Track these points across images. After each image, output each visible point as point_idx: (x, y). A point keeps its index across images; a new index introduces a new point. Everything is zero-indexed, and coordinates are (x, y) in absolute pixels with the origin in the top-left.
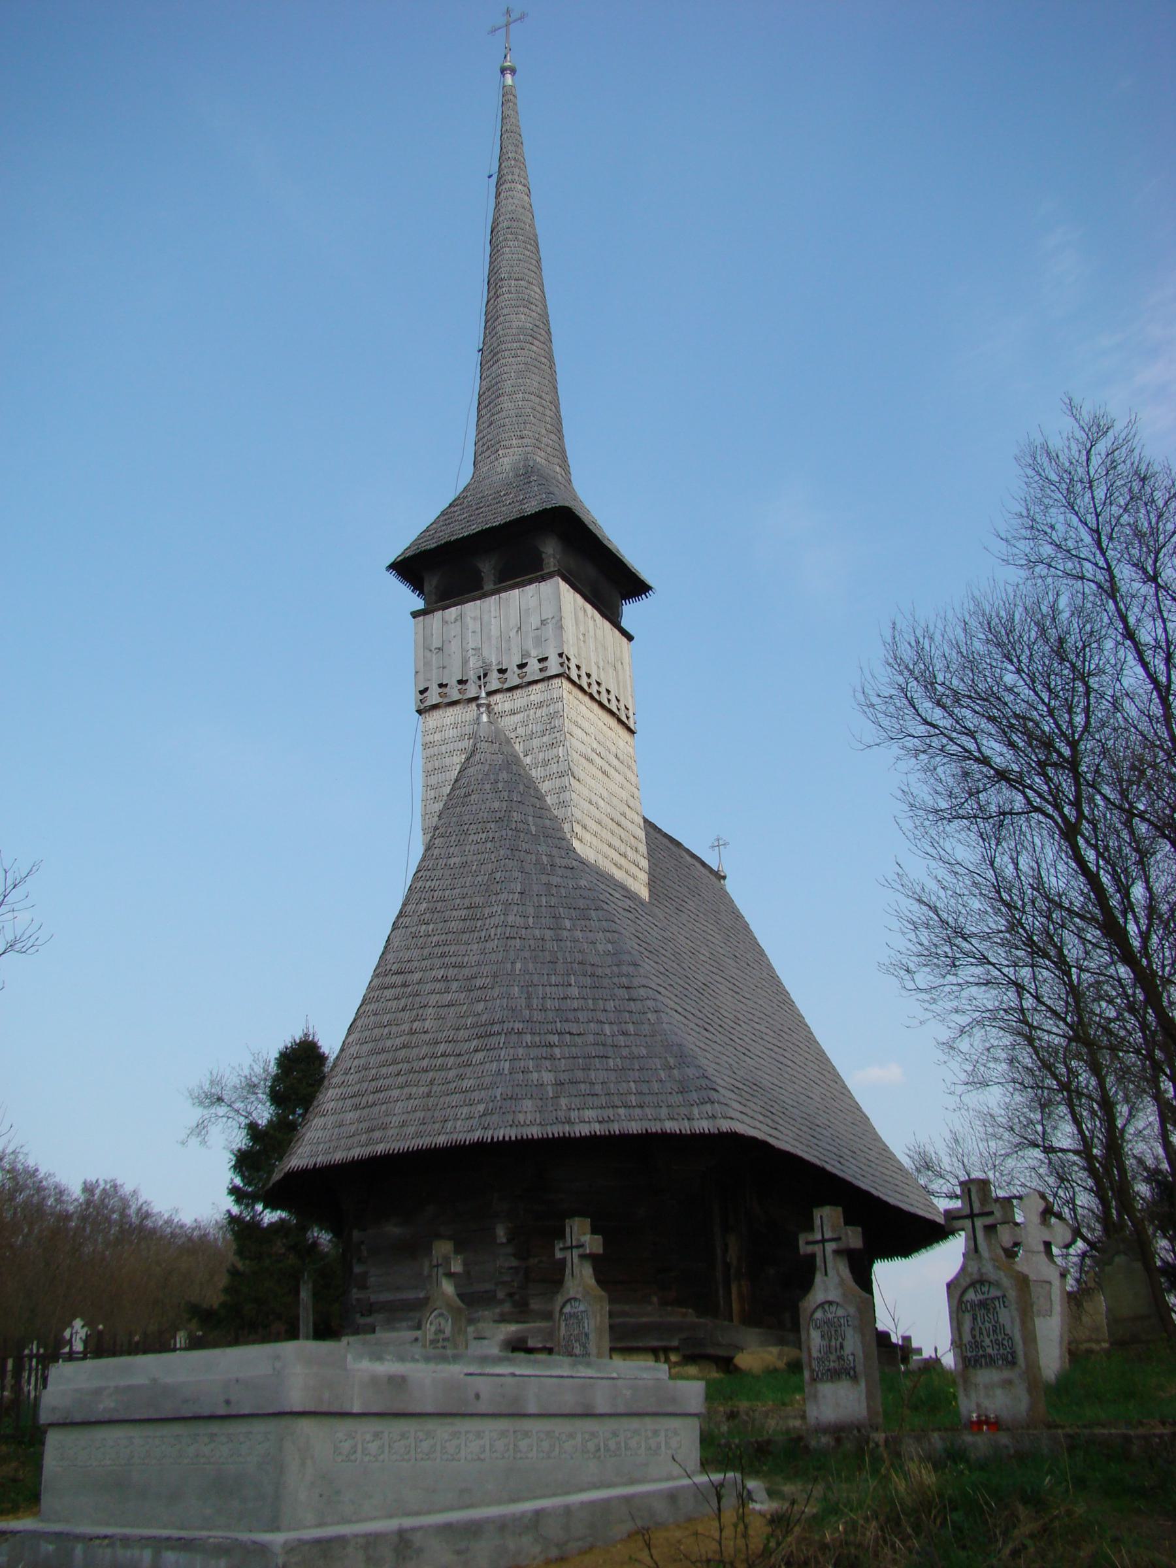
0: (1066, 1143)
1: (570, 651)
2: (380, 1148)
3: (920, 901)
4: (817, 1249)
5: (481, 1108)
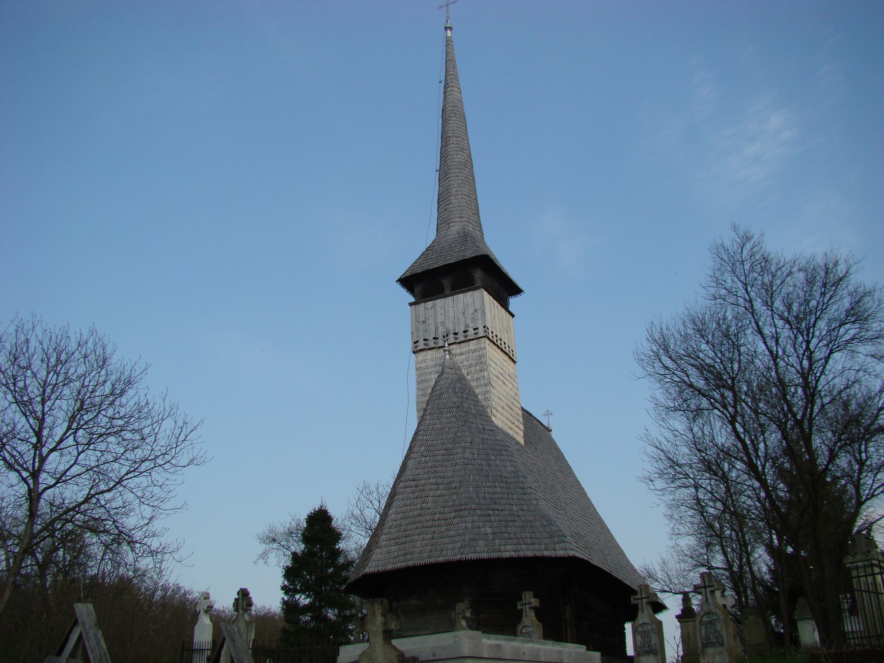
0: (719, 565)
1: (489, 325)
2: (411, 563)
3: (656, 447)
4: (639, 601)
5: (459, 544)
